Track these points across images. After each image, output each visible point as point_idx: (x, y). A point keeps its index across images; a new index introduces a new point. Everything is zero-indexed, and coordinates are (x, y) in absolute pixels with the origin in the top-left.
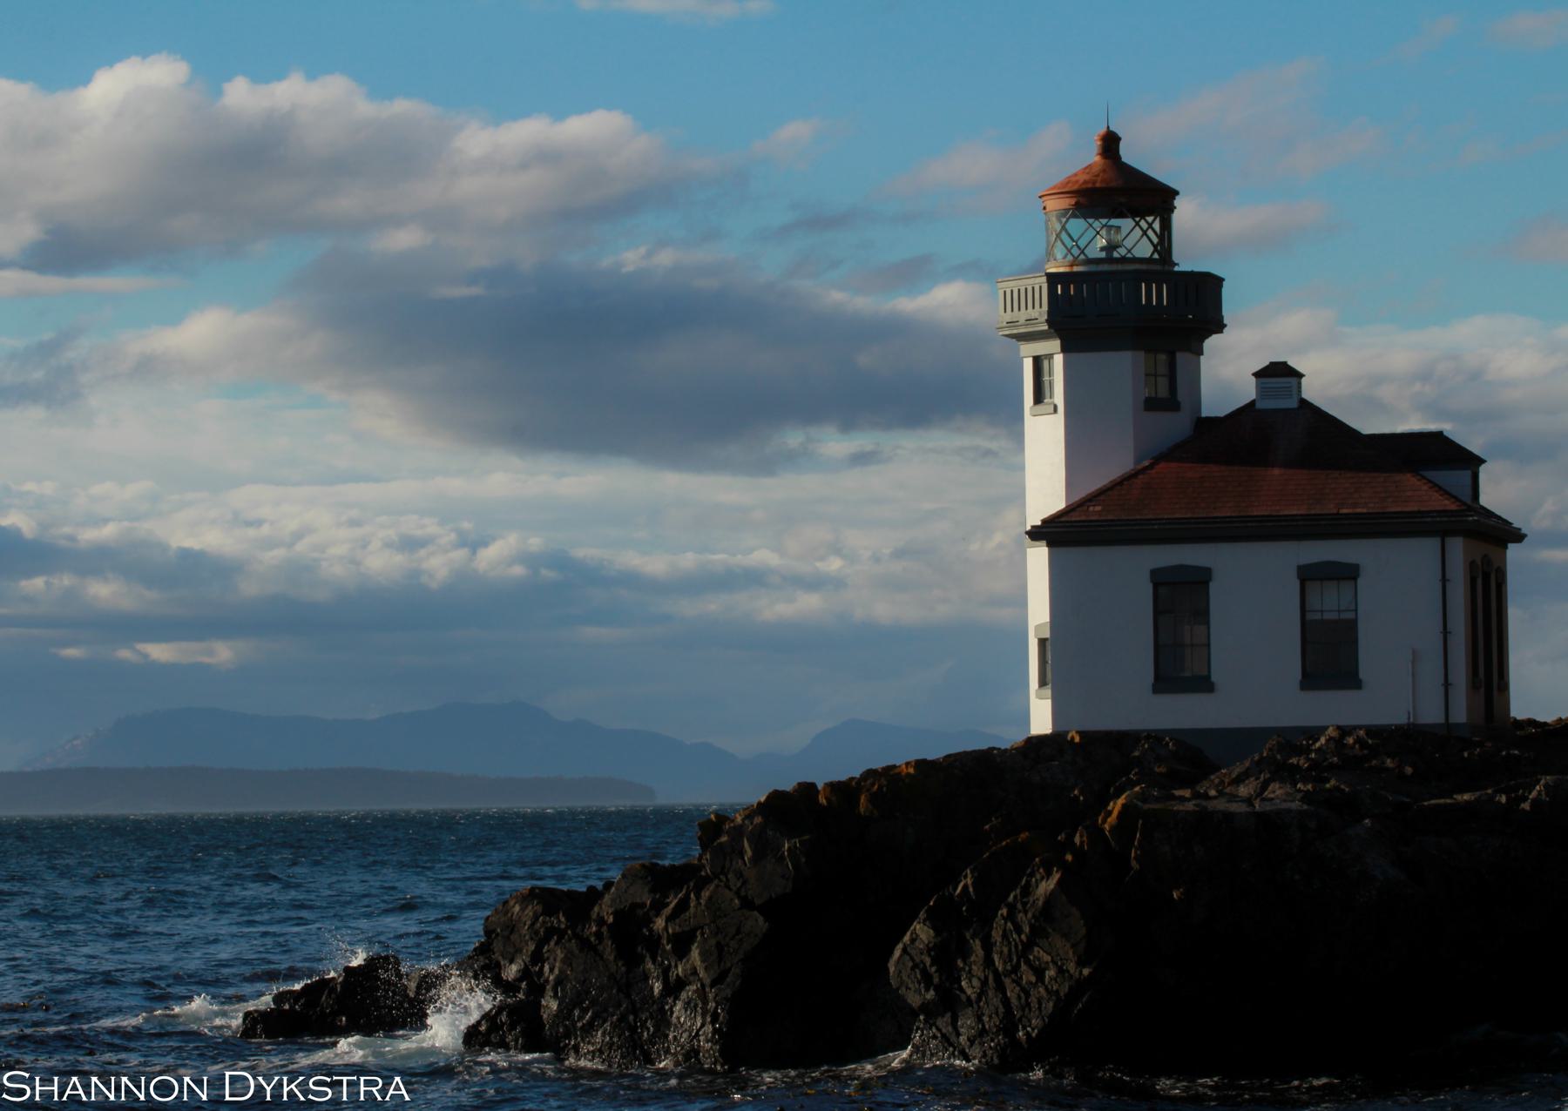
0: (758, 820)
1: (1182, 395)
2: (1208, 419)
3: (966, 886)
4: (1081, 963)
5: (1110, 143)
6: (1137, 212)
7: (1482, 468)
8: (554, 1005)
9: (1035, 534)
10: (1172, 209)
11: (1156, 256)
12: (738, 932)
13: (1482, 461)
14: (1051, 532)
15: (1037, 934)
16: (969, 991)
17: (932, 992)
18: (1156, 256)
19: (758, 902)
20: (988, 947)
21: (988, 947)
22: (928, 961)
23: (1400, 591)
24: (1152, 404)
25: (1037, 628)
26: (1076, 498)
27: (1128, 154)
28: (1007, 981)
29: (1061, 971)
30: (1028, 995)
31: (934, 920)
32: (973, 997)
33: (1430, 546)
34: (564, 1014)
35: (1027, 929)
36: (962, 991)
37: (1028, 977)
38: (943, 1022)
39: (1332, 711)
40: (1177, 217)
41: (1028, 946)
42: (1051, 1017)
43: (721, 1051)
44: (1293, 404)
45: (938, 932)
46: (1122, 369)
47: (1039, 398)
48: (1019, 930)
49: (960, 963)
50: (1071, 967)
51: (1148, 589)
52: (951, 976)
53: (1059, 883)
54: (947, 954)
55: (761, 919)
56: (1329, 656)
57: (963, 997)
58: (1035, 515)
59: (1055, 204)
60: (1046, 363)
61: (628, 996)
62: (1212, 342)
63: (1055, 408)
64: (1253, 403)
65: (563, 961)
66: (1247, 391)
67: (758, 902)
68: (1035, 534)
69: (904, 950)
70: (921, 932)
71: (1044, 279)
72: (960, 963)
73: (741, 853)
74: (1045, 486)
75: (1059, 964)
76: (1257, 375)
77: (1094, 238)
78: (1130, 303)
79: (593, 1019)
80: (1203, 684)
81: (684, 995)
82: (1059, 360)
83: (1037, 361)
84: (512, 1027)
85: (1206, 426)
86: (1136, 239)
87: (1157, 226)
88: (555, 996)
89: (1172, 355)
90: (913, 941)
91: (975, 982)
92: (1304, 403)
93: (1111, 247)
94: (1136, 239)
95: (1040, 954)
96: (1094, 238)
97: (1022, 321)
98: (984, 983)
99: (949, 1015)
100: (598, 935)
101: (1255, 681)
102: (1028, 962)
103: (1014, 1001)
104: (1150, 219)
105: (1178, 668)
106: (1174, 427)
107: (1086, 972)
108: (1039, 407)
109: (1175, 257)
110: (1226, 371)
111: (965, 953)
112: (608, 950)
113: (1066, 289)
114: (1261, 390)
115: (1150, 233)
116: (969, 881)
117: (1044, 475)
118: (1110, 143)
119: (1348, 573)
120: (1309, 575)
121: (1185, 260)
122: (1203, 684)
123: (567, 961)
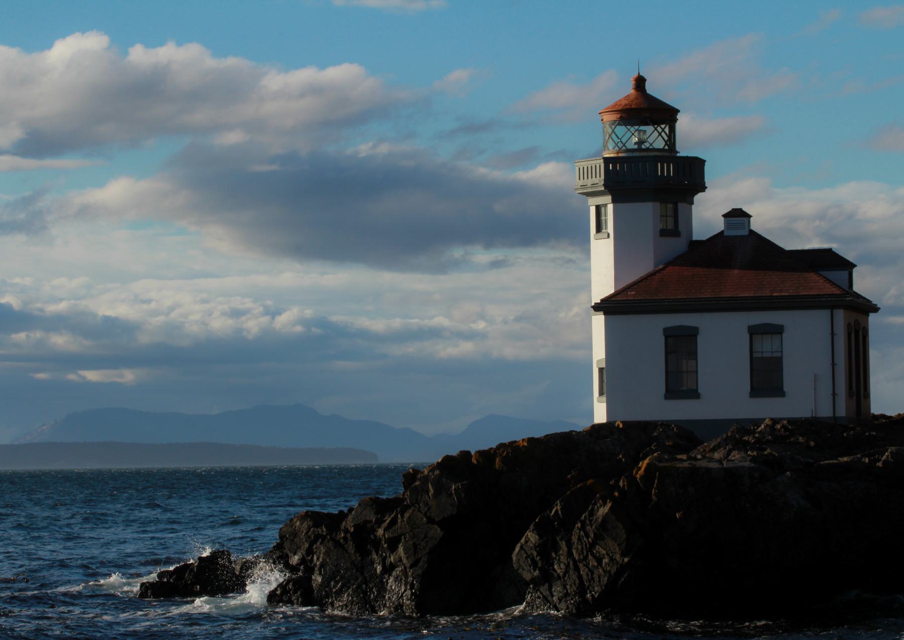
0: (437, 472)
1: (681, 227)
2: (696, 241)
3: (557, 511)
4: (623, 555)
5: (640, 82)
6: (655, 122)
7: (855, 270)
8: (319, 579)
9: (597, 308)
10: (676, 120)
11: (666, 147)
12: (426, 537)
13: (855, 266)
14: (606, 306)
15: (598, 538)
16: (559, 571)
17: (537, 572)
18: (666, 147)
19: (437, 519)
20: (569, 545)
21: (569, 545)
22: (535, 554)
23: (807, 341)
24: (664, 233)
25: (598, 361)
26: (621, 287)
27: (650, 89)
28: (581, 565)
29: (611, 559)
30: (592, 573)
31: (539, 530)
32: (561, 574)
33: (824, 314)
34: (325, 584)
35: (592, 535)
36: (555, 571)
37: (593, 563)
38: (544, 589)
39: (768, 409)
40: (678, 125)
41: (593, 545)
42: (606, 586)
43: (415, 606)
44: (746, 233)
45: (541, 537)
46: (647, 213)
47: (599, 229)
48: (587, 535)
49: (553, 555)
50: (618, 557)
51: (662, 339)
52: (548, 562)
53: (611, 509)
54: (546, 550)
55: (439, 529)
56: (766, 378)
57: (555, 575)
58: (597, 297)
59: (608, 118)
60: (603, 209)
61: (362, 573)
62: (699, 197)
63: (609, 235)
64: (722, 232)
65: (324, 554)
66: (719, 225)
67: (437, 519)
68: (597, 308)
69: (521, 547)
70: (531, 537)
71: (602, 161)
72: (553, 555)
73: (427, 491)
74: (603, 280)
75: (611, 555)
76: (725, 216)
77: (631, 137)
78: (652, 175)
79: (342, 587)
80: (694, 394)
81: (394, 573)
82: (610, 207)
83: (598, 208)
84: (295, 592)
85: (695, 245)
86: (655, 138)
87: (667, 130)
88: (320, 574)
89: (676, 205)
90: (526, 542)
91: (562, 566)
92: (752, 232)
93: (640, 142)
94: (655, 138)
95: (600, 550)
96: (631, 137)
97: (589, 185)
98: (567, 566)
99: (547, 585)
100: (345, 538)
101: (723, 392)
102: (592, 554)
103: (585, 577)
104: (663, 126)
105: (679, 385)
106: (677, 246)
107: (626, 560)
108: (599, 234)
109: (678, 148)
110: (707, 214)
111: (556, 549)
112: (351, 547)
113: (614, 167)
114: (727, 224)
115: (663, 134)
116: (559, 508)
117: (602, 273)
118: (640, 82)
119: (777, 330)
120: (755, 331)
121: (683, 150)
122: (694, 394)
123: (327, 554)
